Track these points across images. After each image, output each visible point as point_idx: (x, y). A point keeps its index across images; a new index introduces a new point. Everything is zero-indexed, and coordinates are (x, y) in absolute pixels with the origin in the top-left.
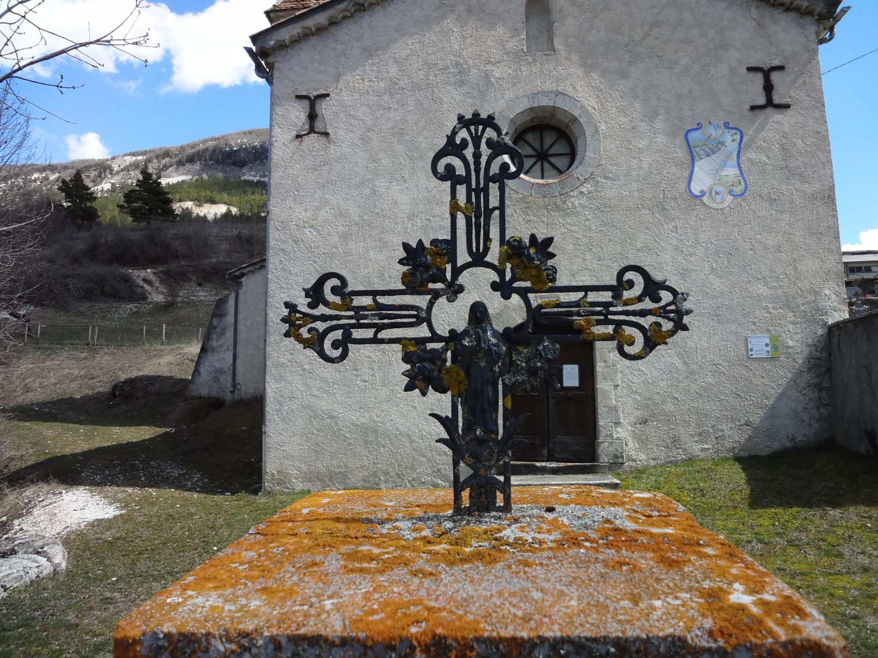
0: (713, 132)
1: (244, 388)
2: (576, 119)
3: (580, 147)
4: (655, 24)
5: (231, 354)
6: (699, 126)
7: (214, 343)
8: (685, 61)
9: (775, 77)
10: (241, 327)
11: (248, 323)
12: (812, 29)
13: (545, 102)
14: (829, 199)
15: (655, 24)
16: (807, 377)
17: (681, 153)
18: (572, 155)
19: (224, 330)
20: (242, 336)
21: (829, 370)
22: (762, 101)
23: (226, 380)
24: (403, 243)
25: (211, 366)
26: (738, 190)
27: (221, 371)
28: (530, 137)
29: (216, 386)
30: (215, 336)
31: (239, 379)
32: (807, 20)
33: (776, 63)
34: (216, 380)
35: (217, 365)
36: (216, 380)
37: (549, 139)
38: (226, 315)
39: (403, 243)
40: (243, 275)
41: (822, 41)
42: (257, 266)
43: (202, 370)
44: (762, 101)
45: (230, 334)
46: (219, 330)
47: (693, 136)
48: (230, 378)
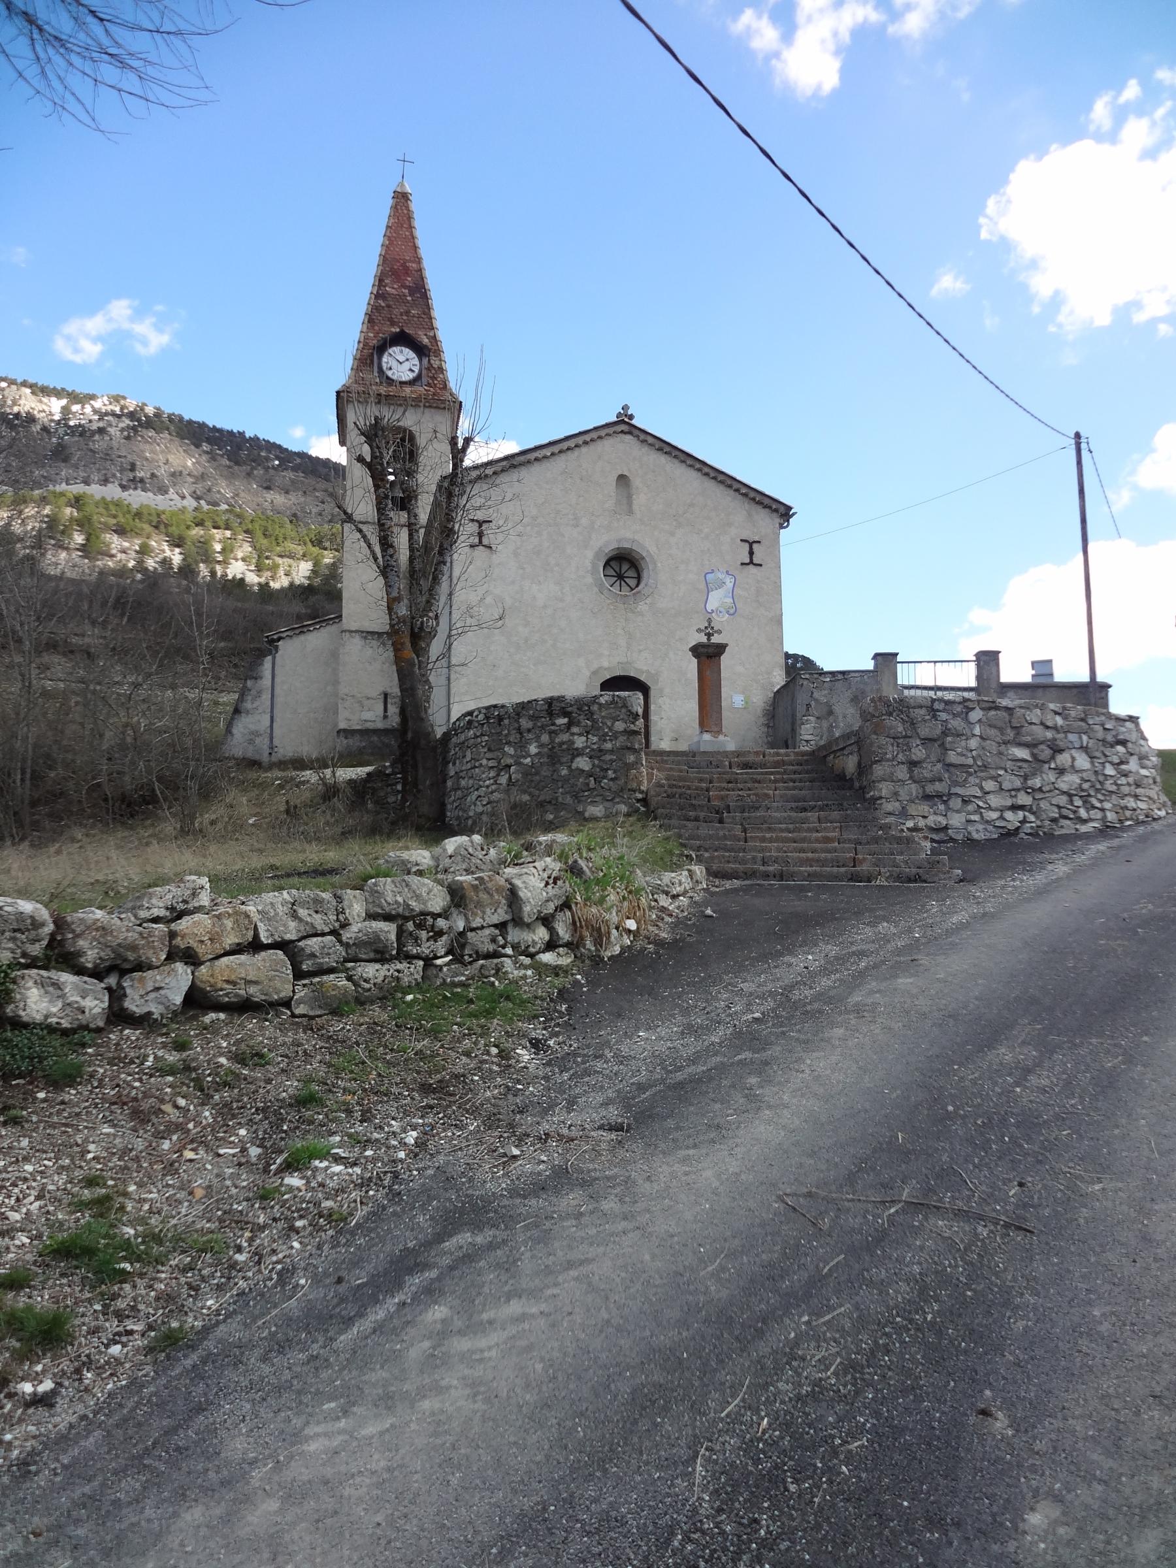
0: (721, 576)
1: (281, 751)
2: (643, 558)
3: (645, 574)
4: (692, 505)
5: (268, 717)
6: (713, 572)
7: (248, 705)
8: (706, 530)
9: (755, 546)
10: (278, 691)
11: (285, 687)
12: (778, 521)
13: (626, 545)
14: (779, 622)
15: (692, 505)
16: (762, 720)
17: (703, 586)
18: (639, 579)
19: (260, 692)
20: (279, 700)
21: (773, 717)
22: (748, 561)
23: (263, 743)
24: (726, 645)
25: (245, 728)
26: (732, 611)
27: (256, 734)
28: (613, 563)
29: (251, 747)
30: (250, 698)
31: (276, 742)
32: (775, 514)
33: (756, 539)
34: (251, 742)
35: (252, 727)
36: (251, 742)
37: (625, 567)
38: (261, 678)
39: (726, 645)
40: (279, 639)
41: (781, 527)
42: (297, 631)
43: (235, 731)
44: (748, 561)
45: (266, 696)
46: (253, 692)
47: (709, 576)
48: (267, 741)
